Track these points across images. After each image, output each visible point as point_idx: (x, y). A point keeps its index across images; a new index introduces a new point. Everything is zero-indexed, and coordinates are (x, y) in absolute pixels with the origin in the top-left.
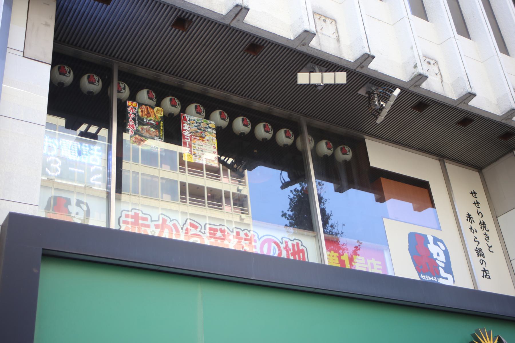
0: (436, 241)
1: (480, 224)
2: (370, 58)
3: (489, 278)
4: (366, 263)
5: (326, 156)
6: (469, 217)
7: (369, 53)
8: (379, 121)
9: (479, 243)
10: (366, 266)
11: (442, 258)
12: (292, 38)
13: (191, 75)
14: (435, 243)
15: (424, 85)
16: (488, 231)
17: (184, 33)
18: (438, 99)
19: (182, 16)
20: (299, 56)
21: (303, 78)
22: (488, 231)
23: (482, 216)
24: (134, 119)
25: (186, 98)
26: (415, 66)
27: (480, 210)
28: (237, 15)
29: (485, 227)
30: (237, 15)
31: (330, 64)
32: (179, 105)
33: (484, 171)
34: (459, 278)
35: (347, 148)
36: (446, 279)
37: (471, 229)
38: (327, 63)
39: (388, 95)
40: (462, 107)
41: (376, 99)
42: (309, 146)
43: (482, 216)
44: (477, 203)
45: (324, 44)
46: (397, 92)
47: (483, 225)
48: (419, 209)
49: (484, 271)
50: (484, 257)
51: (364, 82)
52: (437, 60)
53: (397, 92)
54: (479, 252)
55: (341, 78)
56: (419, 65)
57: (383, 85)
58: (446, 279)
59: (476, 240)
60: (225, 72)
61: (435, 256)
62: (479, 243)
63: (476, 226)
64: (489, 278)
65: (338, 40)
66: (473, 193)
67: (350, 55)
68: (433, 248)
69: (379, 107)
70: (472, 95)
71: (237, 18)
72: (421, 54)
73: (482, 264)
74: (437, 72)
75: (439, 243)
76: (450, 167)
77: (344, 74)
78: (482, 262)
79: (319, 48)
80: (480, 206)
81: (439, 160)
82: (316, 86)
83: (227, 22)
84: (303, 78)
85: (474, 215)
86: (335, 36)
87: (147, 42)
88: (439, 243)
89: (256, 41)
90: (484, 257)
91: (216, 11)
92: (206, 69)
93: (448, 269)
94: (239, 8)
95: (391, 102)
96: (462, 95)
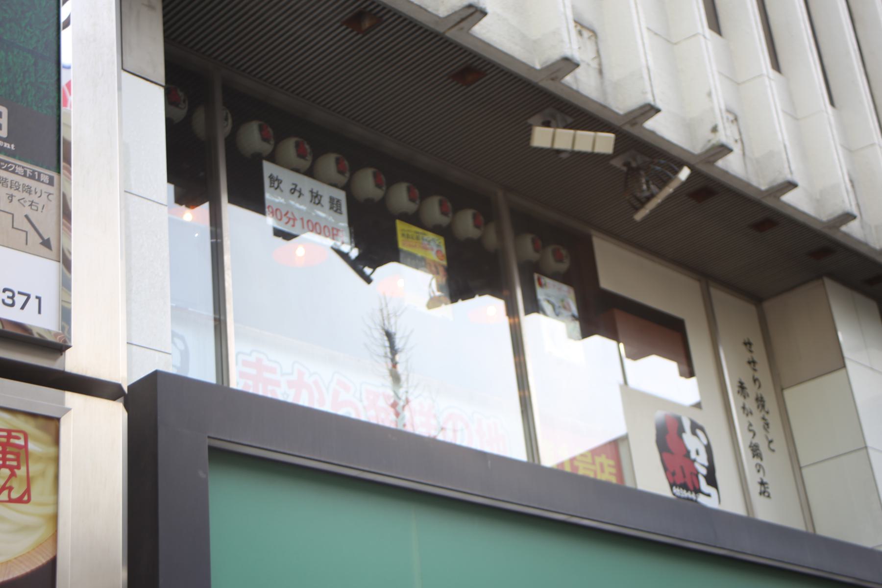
0: (695, 427)
1: (757, 399)
2: (478, 15)
3: (769, 496)
4: (594, 463)
5: (369, 201)
6: (742, 387)
7: (652, 103)
8: (639, 216)
9: (754, 435)
10: (592, 467)
11: (702, 459)
12: (538, 67)
13: (287, 80)
14: (694, 433)
15: (568, 79)
16: (768, 412)
17: (360, 36)
18: (665, 147)
19: (484, 69)
20: (542, 96)
21: (542, 137)
22: (768, 412)
23: (760, 386)
24: (403, 235)
25: (425, 184)
26: (715, 130)
27: (757, 375)
28: (463, 20)
29: (763, 406)
30: (463, 20)
31: (456, 46)
32: (184, 101)
33: (767, 305)
34: (725, 498)
35: (564, 252)
36: (709, 495)
37: (744, 408)
38: (389, 11)
39: (668, 175)
40: (769, 202)
41: (644, 180)
42: (223, 129)
43: (760, 386)
44: (752, 362)
45: (584, 83)
46: (684, 174)
47: (760, 401)
48: (682, 374)
49: (762, 483)
50: (762, 459)
51: (641, 154)
52: (739, 114)
53: (684, 174)
54: (755, 451)
55: (603, 143)
56: (720, 127)
57: (656, 158)
58: (709, 495)
59: (751, 428)
60: (293, 51)
61: (693, 455)
62: (754, 435)
63: (751, 404)
64: (769, 496)
65: (600, 72)
66: (748, 344)
67: (621, 103)
68: (692, 443)
69: (647, 194)
70: (791, 185)
71: (462, 24)
72: (723, 107)
73: (759, 471)
74: (737, 137)
75: (699, 432)
76: (718, 295)
77: (612, 136)
78: (759, 468)
79: (574, 87)
80: (757, 367)
81: (699, 280)
82: (559, 152)
83: (440, 29)
84: (542, 137)
85: (749, 384)
86: (594, 64)
87: (264, 31)
88: (699, 432)
89: (476, 64)
90: (762, 459)
91: (430, 10)
92: (312, 66)
93: (712, 480)
94: (471, 10)
95: (669, 190)
96: (775, 184)
